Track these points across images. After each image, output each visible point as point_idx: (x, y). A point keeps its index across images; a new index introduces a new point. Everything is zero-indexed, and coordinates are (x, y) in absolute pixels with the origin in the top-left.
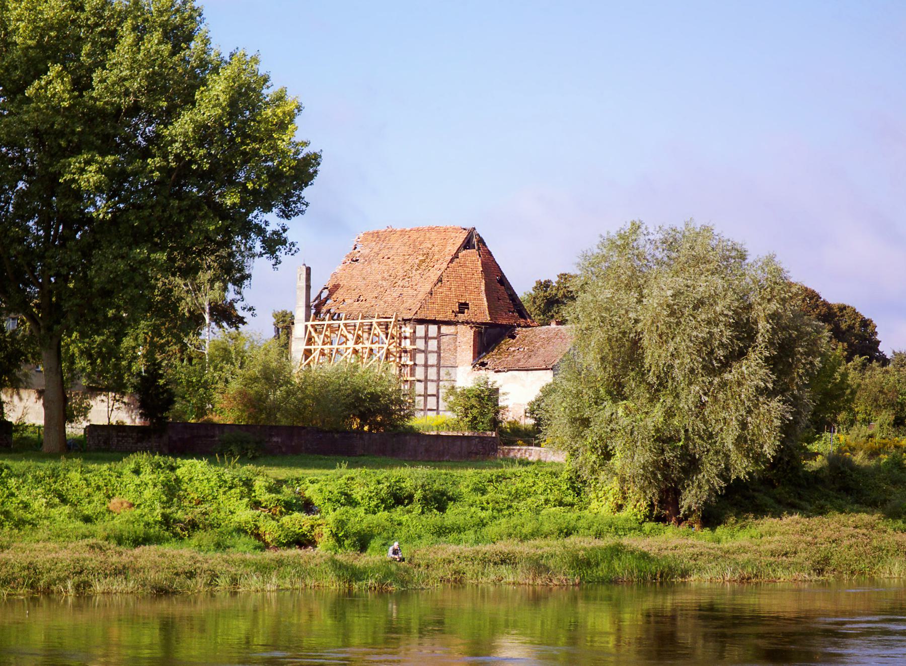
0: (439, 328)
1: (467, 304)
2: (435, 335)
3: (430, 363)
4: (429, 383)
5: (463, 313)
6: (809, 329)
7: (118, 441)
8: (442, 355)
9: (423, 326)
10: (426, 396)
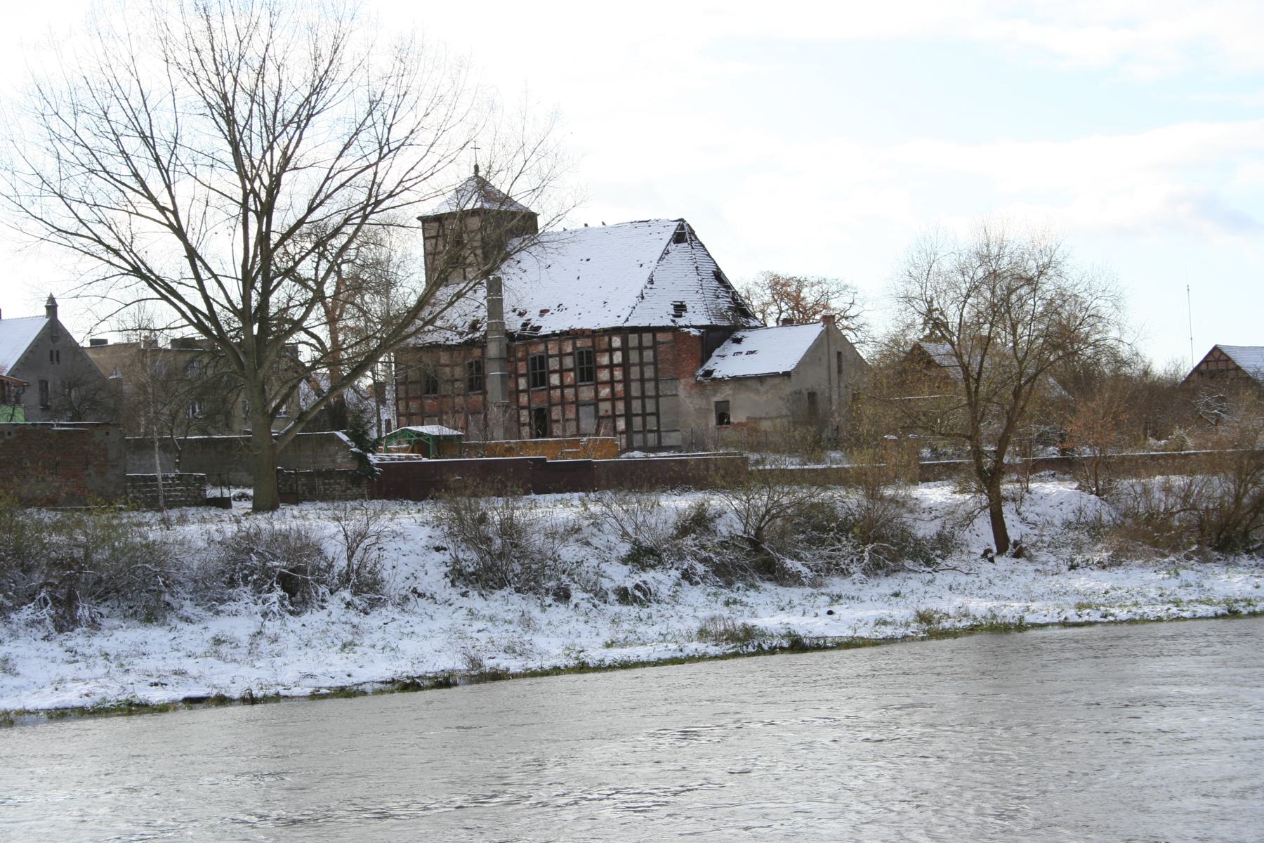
0: (654, 337)
1: (684, 306)
2: (650, 344)
3: (639, 402)
4: (647, 400)
5: (681, 316)
6: (210, 372)
7: (325, 490)
8: (660, 366)
9: (636, 335)
10: (644, 415)
